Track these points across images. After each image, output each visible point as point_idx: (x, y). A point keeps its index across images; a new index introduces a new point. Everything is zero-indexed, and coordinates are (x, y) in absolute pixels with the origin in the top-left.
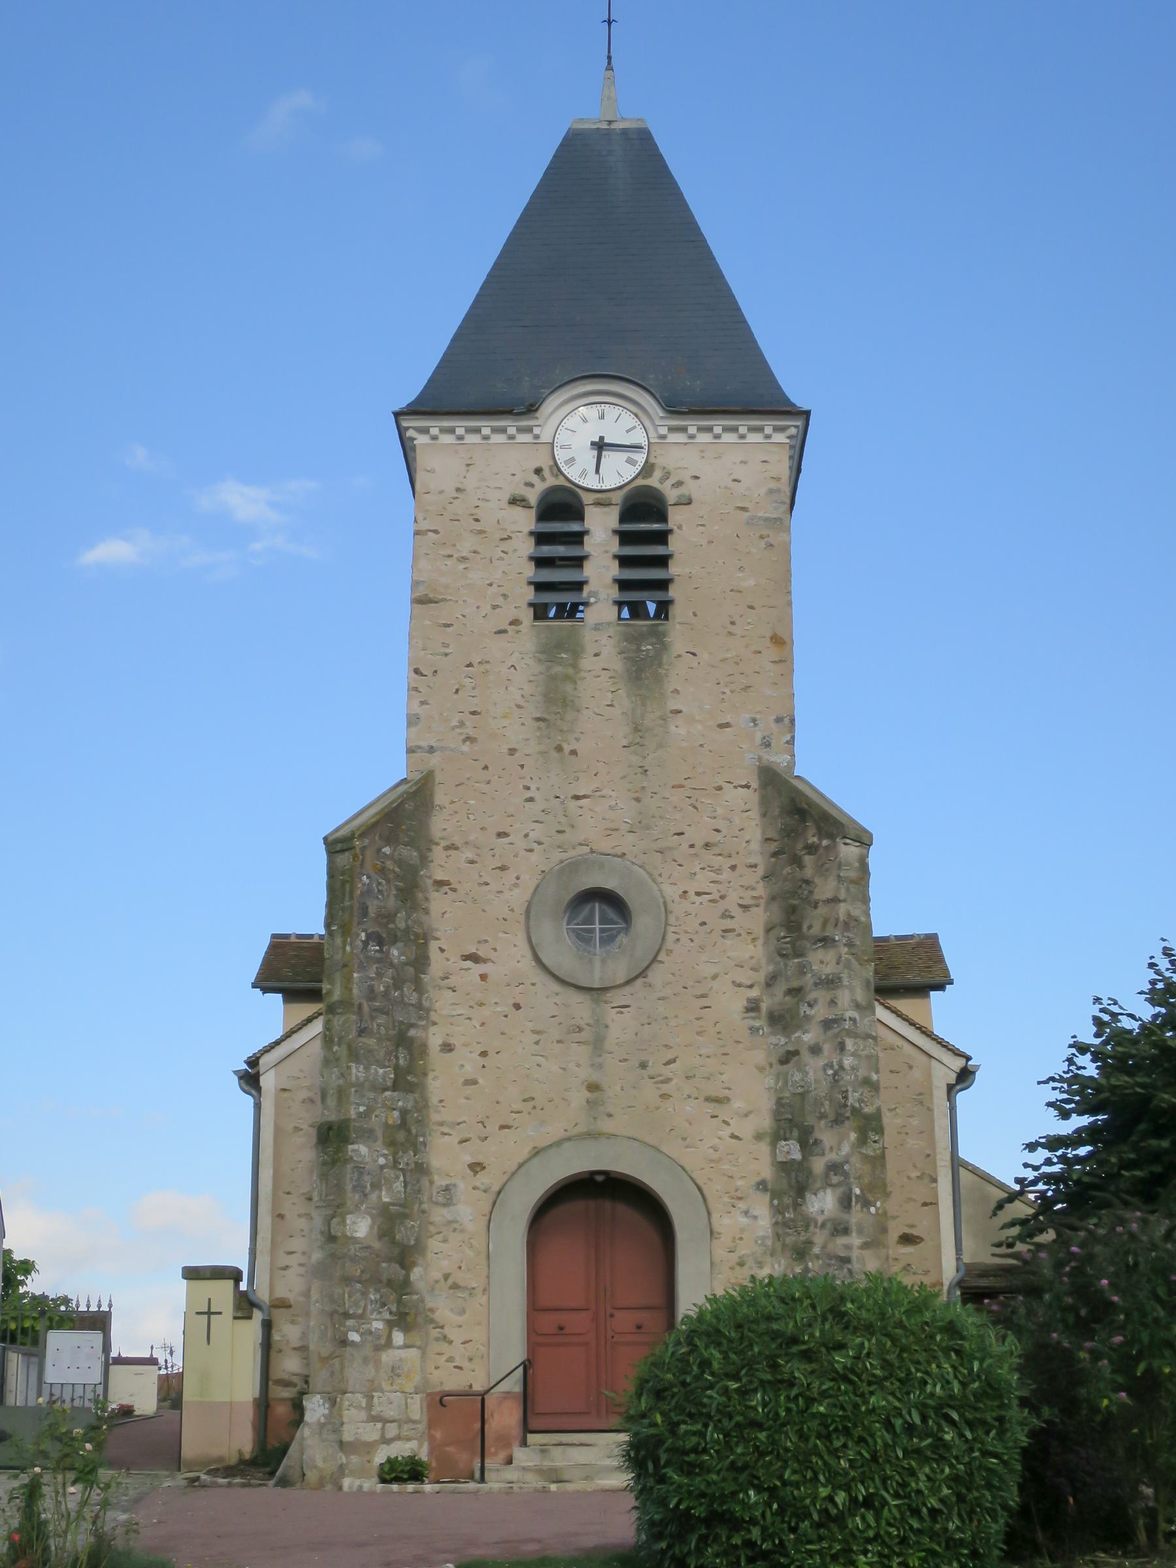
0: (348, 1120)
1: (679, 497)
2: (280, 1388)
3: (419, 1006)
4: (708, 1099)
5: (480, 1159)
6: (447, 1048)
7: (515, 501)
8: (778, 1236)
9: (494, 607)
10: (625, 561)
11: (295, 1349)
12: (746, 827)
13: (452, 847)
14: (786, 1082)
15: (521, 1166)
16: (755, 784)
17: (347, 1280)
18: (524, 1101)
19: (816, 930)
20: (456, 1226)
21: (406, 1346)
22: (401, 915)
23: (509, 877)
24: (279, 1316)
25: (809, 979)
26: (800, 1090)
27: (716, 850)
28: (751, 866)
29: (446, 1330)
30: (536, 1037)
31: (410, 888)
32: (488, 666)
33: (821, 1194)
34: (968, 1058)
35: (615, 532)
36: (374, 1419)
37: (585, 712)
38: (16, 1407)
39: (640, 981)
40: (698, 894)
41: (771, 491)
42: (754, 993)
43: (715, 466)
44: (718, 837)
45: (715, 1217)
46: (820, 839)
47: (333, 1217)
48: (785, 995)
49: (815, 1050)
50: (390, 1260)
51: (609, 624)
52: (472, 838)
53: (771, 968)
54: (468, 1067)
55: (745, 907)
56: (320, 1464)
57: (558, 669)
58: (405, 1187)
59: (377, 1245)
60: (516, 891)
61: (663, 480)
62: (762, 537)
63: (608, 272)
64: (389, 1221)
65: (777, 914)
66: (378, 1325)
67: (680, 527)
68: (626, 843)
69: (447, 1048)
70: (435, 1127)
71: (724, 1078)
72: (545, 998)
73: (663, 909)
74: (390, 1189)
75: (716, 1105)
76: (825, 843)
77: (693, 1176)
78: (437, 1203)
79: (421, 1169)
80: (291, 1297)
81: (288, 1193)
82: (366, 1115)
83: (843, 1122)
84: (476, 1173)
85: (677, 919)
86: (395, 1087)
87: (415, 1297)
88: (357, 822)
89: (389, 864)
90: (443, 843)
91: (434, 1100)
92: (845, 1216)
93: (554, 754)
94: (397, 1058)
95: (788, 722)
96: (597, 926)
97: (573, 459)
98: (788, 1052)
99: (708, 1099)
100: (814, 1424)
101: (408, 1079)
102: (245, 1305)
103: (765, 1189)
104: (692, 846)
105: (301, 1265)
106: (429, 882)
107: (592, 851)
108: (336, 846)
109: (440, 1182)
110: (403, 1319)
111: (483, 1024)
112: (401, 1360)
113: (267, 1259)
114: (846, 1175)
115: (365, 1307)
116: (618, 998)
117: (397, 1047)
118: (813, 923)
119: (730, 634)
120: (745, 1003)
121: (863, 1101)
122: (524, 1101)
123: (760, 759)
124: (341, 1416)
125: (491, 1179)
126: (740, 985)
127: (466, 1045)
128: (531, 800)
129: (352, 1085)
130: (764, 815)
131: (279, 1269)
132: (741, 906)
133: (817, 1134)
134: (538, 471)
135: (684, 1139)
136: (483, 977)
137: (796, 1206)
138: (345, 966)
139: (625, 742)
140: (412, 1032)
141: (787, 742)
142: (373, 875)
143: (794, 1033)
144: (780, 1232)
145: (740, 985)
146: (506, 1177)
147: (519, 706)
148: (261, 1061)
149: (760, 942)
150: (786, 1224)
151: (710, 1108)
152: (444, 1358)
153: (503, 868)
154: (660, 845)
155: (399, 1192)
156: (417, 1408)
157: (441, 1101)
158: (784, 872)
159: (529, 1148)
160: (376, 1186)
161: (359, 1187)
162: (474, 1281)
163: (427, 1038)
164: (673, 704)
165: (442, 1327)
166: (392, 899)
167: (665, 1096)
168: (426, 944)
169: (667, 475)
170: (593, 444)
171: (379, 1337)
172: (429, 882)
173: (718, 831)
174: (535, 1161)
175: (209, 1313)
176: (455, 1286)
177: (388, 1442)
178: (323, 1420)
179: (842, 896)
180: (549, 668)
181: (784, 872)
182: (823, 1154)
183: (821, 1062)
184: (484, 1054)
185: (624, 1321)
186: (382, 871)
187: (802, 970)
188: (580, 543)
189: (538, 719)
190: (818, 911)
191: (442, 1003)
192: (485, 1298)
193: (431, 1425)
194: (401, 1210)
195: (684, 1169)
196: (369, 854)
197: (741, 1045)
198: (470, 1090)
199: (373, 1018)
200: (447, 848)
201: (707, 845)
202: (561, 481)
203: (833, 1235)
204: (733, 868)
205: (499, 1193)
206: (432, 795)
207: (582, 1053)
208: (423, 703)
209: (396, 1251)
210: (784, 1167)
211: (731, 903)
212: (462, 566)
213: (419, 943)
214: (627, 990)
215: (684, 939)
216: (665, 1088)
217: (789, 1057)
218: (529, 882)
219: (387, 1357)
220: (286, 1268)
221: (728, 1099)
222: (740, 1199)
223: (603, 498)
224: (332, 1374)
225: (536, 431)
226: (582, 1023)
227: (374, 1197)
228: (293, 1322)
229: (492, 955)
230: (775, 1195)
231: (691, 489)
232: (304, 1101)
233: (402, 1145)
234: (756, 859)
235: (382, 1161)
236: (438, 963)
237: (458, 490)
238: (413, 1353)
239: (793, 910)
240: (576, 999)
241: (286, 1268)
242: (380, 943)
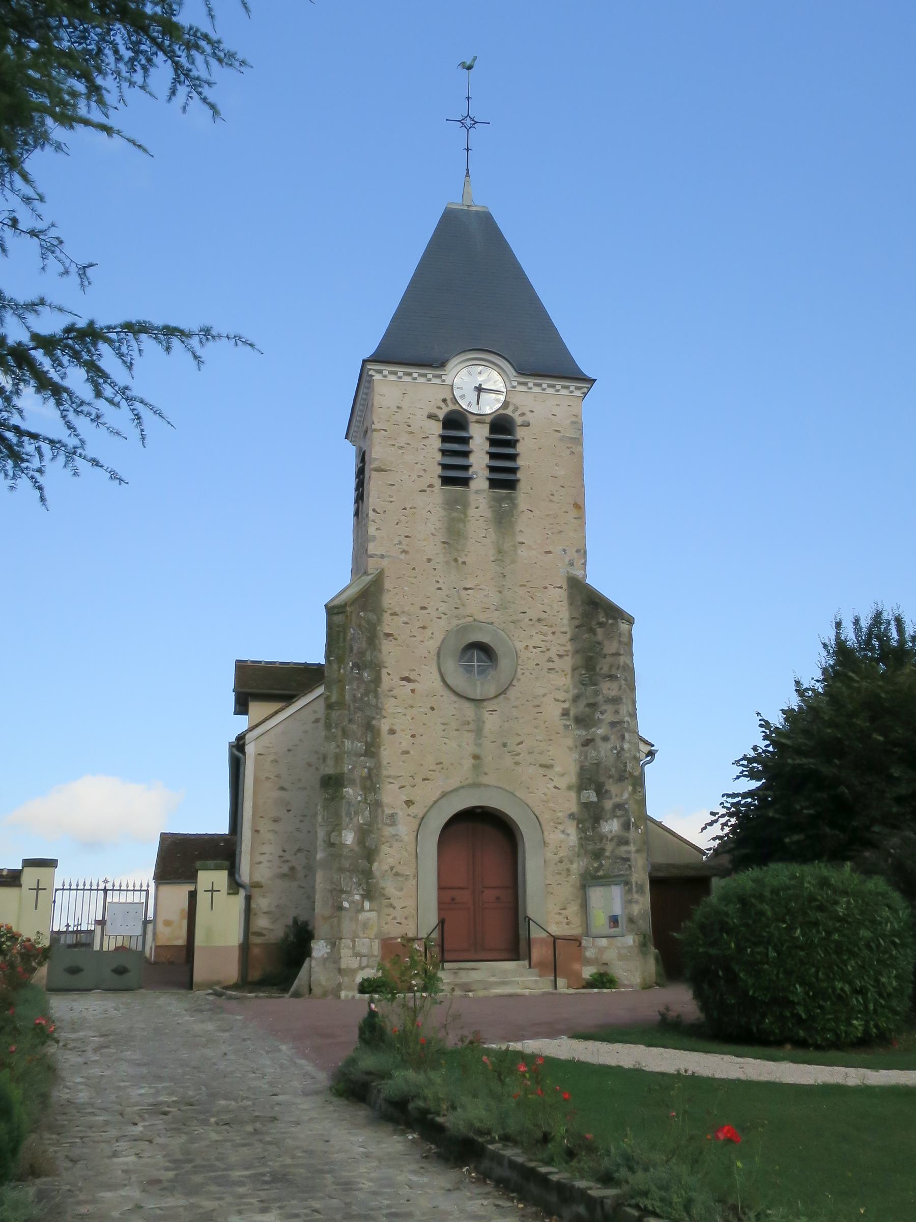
0: (343, 773)
4: (541, 766)
5: (412, 798)
7: (431, 416)
8: (581, 846)
9: (419, 476)
10: (492, 456)
11: (265, 913)
12: (558, 608)
13: (395, 614)
14: (586, 757)
15: (435, 802)
16: (565, 587)
17: (341, 870)
19: (605, 670)
21: (371, 910)
22: (368, 653)
23: (428, 632)
24: (256, 892)
25: (600, 698)
26: (596, 762)
29: (392, 901)
30: (444, 727)
31: (372, 637)
32: (414, 510)
33: (610, 822)
34: (653, 746)
35: (487, 439)
36: (356, 955)
38: (108, 951)
40: (534, 647)
42: (566, 705)
43: (541, 407)
44: (544, 616)
45: (546, 833)
47: (333, 831)
49: (605, 739)
51: (484, 490)
52: (406, 609)
53: (576, 691)
54: (404, 744)
55: (560, 656)
56: (324, 983)
57: (455, 515)
60: (432, 642)
61: (514, 411)
62: (568, 448)
63: (467, 292)
64: (364, 833)
66: (357, 897)
67: (523, 439)
68: (495, 616)
69: (392, 732)
72: (449, 705)
74: (363, 815)
76: (610, 621)
79: (378, 804)
82: (351, 771)
83: (623, 780)
84: (409, 806)
85: (523, 661)
86: (365, 755)
88: (344, 597)
89: (363, 623)
90: (390, 612)
91: (384, 762)
92: (626, 834)
93: (453, 563)
95: (582, 552)
96: (476, 664)
97: (464, 395)
100: (833, 946)
101: (371, 750)
103: (574, 819)
104: (531, 620)
106: (381, 634)
107: (475, 620)
108: (332, 611)
109: (388, 811)
110: (369, 895)
113: (248, 858)
114: (626, 810)
116: (490, 705)
118: (603, 666)
119: (551, 501)
120: (561, 710)
123: (568, 572)
124: (339, 953)
125: (416, 810)
128: (440, 589)
129: (345, 753)
130: (571, 604)
131: (254, 864)
133: (607, 787)
134: (444, 401)
136: (413, 691)
137: (594, 828)
138: (340, 681)
139: (493, 559)
140: (374, 722)
146: (426, 809)
147: (433, 534)
149: (569, 676)
150: (587, 838)
151: (542, 771)
152: (391, 917)
153: (424, 628)
154: (514, 618)
156: (376, 948)
160: (356, 813)
161: (348, 814)
162: (409, 871)
164: (520, 539)
166: (364, 643)
167: (517, 763)
169: (516, 409)
174: (444, 800)
175: (212, 891)
176: (397, 874)
177: (362, 968)
178: (326, 956)
179: (622, 652)
182: (611, 798)
183: (609, 745)
184: (413, 736)
186: (360, 626)
187: (596, 693)
189: (444, 543)
191: (389, 705)
192: (414, 882)
193: (383, 958)
196: (354, 615)
199: (355, 713)
200: (392, 614)
201: (539, 620)
202: (456, 407)
203: (618, 845)
204: (554, 633)
205: (423, 818)
207: (469, 737)
208: (378, 529)
210: (586, 806)
211: (553, 653)
213: (376, 668)
214: (495, 701)
215: (527, 673)
217: (588, 742)
218: (439, 637)
219: (362, 916)
220: (260, 863)
223: (480, 418)
224: (332, 927)
225: (444, 377)
226: (470, 719)
227: (355, 820)
229: (418, 678)
230: (579, 821)
231: (529, 417)
232: (272, 761)
235: (359, 798)
236: (387, 682)
237: (398, 407)
239: (591, 658)
241: (260, 863)
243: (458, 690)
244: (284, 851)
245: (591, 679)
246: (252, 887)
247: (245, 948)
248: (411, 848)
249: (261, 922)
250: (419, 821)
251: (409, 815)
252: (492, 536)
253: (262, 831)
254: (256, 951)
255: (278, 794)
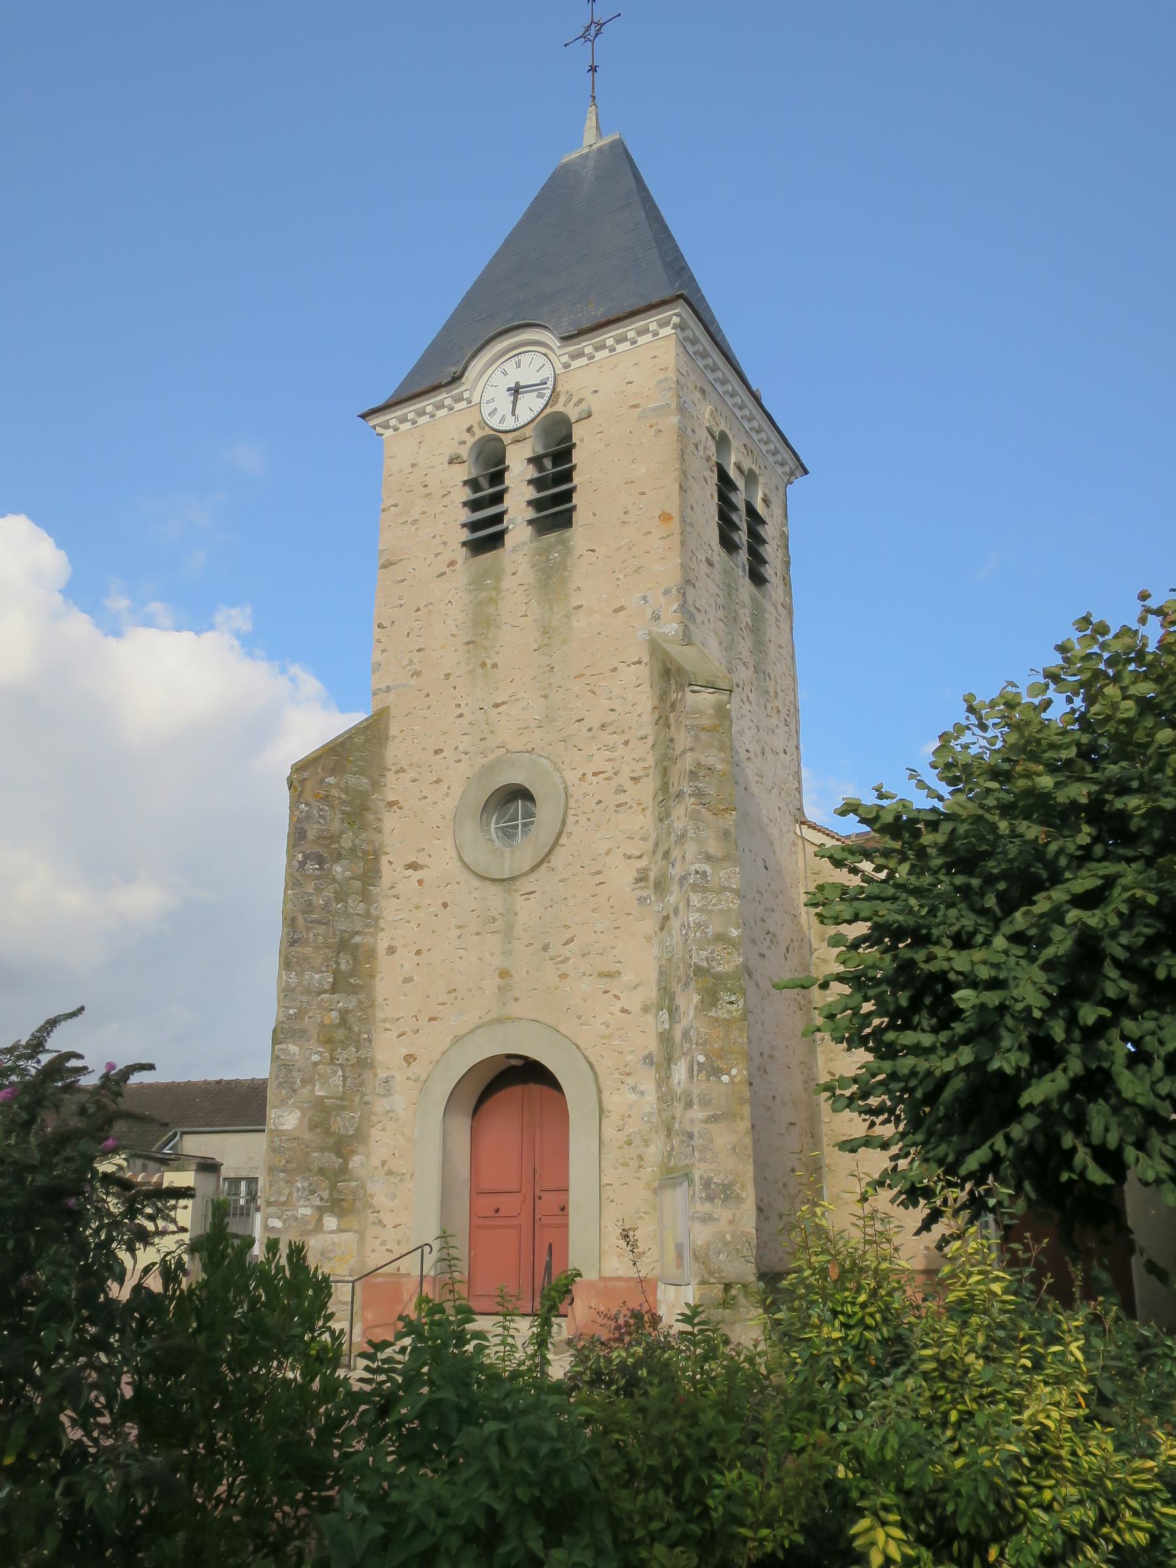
1: (580, 414)
3: (367, 915)
4: (602, 975)
6: (391, 950)
15: (443, 1054)
16: (646, 659)
20: (391, 1115)
21: (340, 1230)
23: (443, 788)
27: (611, 729)
28: (642, 738)
29: (381, 1215)
30: (459, 932)
39: (545, 865)
40: (595, 774)
41: (660, 382)
42: (643, 863)
44: (613, 716)
50: (322, 1150)
55: (635, 780)
57: (484, 595)
58: (344, 1081)
59: (307, 1136)
62: (651, 426)
66: (305, 1211)
67: (582, 440)
71: (616, 951)
73: (563, 795)
75: (608, 979)
77: (587, 1053)
78: (378, 1095)
79: (365, 1064)
86: (334, 989)
87: (354, 1184)
89: (334, 792)
90: (394, 768)
91: (379, 999)
93: (480, 671)
94: (338, 963)
99: (602, 975)
106: (382, 804)
107: (508, 751)
109: (382, 1074)
110: (338, 1205)
112: (333, 1243)
115: (290, 1195)
116: (525, 885)
117: (339, 953)
121: (713, 959)
123: (650, 633)
127: (405, 946)
128: (461, 716)
132: (632, 779)
135: (579, 1017)
140: (357, 939)
142: (313, 802)
145: (630, 857)
151: (603, 984)
152: (379, 1241)
153: (438, 781)
155: (337, 1086)
163: (376, 943)
164: (575, 602)
165: (378, 1212)
167: (563, 976)
168: (377, 859)
170: (509, 389)
171: (306, 1223)
172: (382, 804)
173: (613, 710)
176: (390, 1173)
186: (326, 799)
188: (570, 499)
189: (468, 643)
191: (389, 909)
194: (338, 1102)
195: (578, 1047)
199: (308, 929)
200: (397, 772)
206: (387, 728)
209: (332, 1141)
211: (624, 779)
214: (534, 876)
215: (582, 819)
216: (564, 968)
218: (457, 789)
221: (619, 973)
222: (629, 1074)
226: (496, 913)
233: (342, 1042)
235: (316, 1058)
236: (388, 873)
238: (349, 1236)
240: (493, 890)
242: (320, 860)
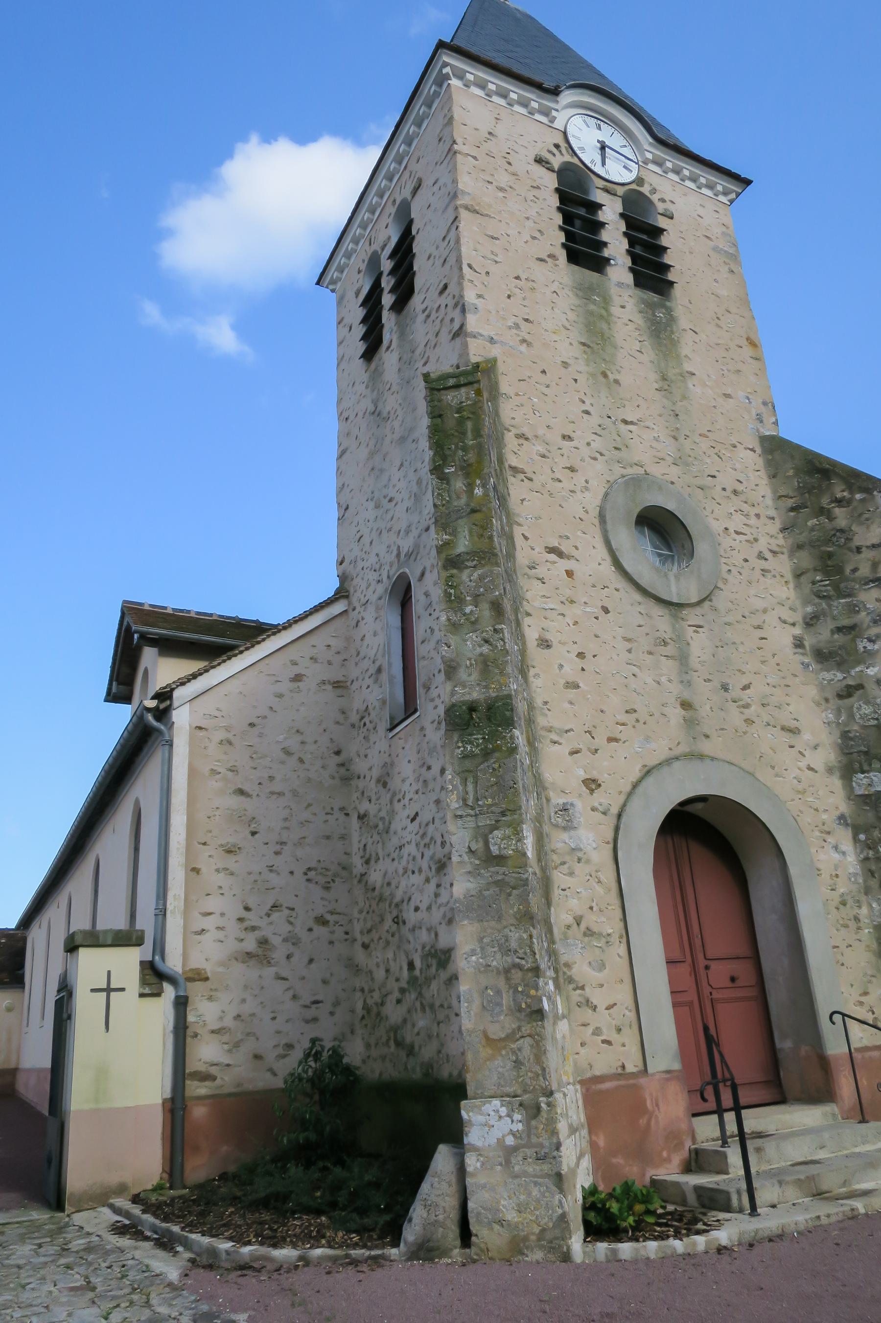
2: (196, 1083)
4: (783, 728)
5: (595, 775)
11: (213, 1032)
14: (851, 716)
15: (635, 786)
18: (627, 712)
24: (195, 990)
25: (863, 617)
30: (628, 645)
37: (621, 350)
40: (737, 533)
46: (852, 492)
47: (494, 828)
48: (833, 632)
52: (540, 432)
53: (809, 609)
54: (567, 668)
55: (774, 553)
56: (511, 1216)
65: (806, 559)
70: (543, 733)
71: (791, 708)
75: (791, 734)
76: (858, 496)
78: (556, 826)
80: (209, 968)
81: (205, 844)
84: (592, 791)
90: (514, 431)
98: (848, 687)
102: (153, 979)
104: (724, 489)
105: (218, 928)
111: (576, 623)
116: (692, 616)
122: (627, 712)
126: (785, 622)
131: (194, 934)
134: (557, 146)
135: (773, 768)
139: (657, 386)
141: (774, 423)
143: (854, 668)
144: (873, 868)
145: (785, 622)
146: (622, 798)
148: (176, 694)
149: (791, 585)
151: (786, 738)
152: (590, 1030)
154: (699, 482)
157: (546, 703)
158: (809, 523)
159: (638, 767)
165: (582, 988)
167: (749, 721)
174: (650, 780)
176: (589, 933)
178: (510, 1141)
180: (586, 304)
181: (809, 523)
184: (581, 655)
185: (720, 973)
189: (584, 344)
190: (863, 556)
191: (533, 594)
197: (797, 679)
198: (572, 693)
205: (619, 816)
207: (669, 667)
208: (480, 296)
212: (501, 194)
214: (698, 610)
215: (734, 571)
217: (848, 692)
224: (518, 1063)
228: (210, 998)
229: (574, 552)
230: (856, 830)
232: (221, 742)
234: (772, 512)
237: (490, 133)
239: (830, 555)
243: (643, 582)
244: (247, 909)
245: (836, 587)
246: (189, 980)
247: (176, 1108)
248: (608, 876)
249: (206, 1052)
250: (614, 821)
251: (593, 809)
252: (649, 354)
253: (204, 870)
254: (199, 1112)
255: (235, 802)
